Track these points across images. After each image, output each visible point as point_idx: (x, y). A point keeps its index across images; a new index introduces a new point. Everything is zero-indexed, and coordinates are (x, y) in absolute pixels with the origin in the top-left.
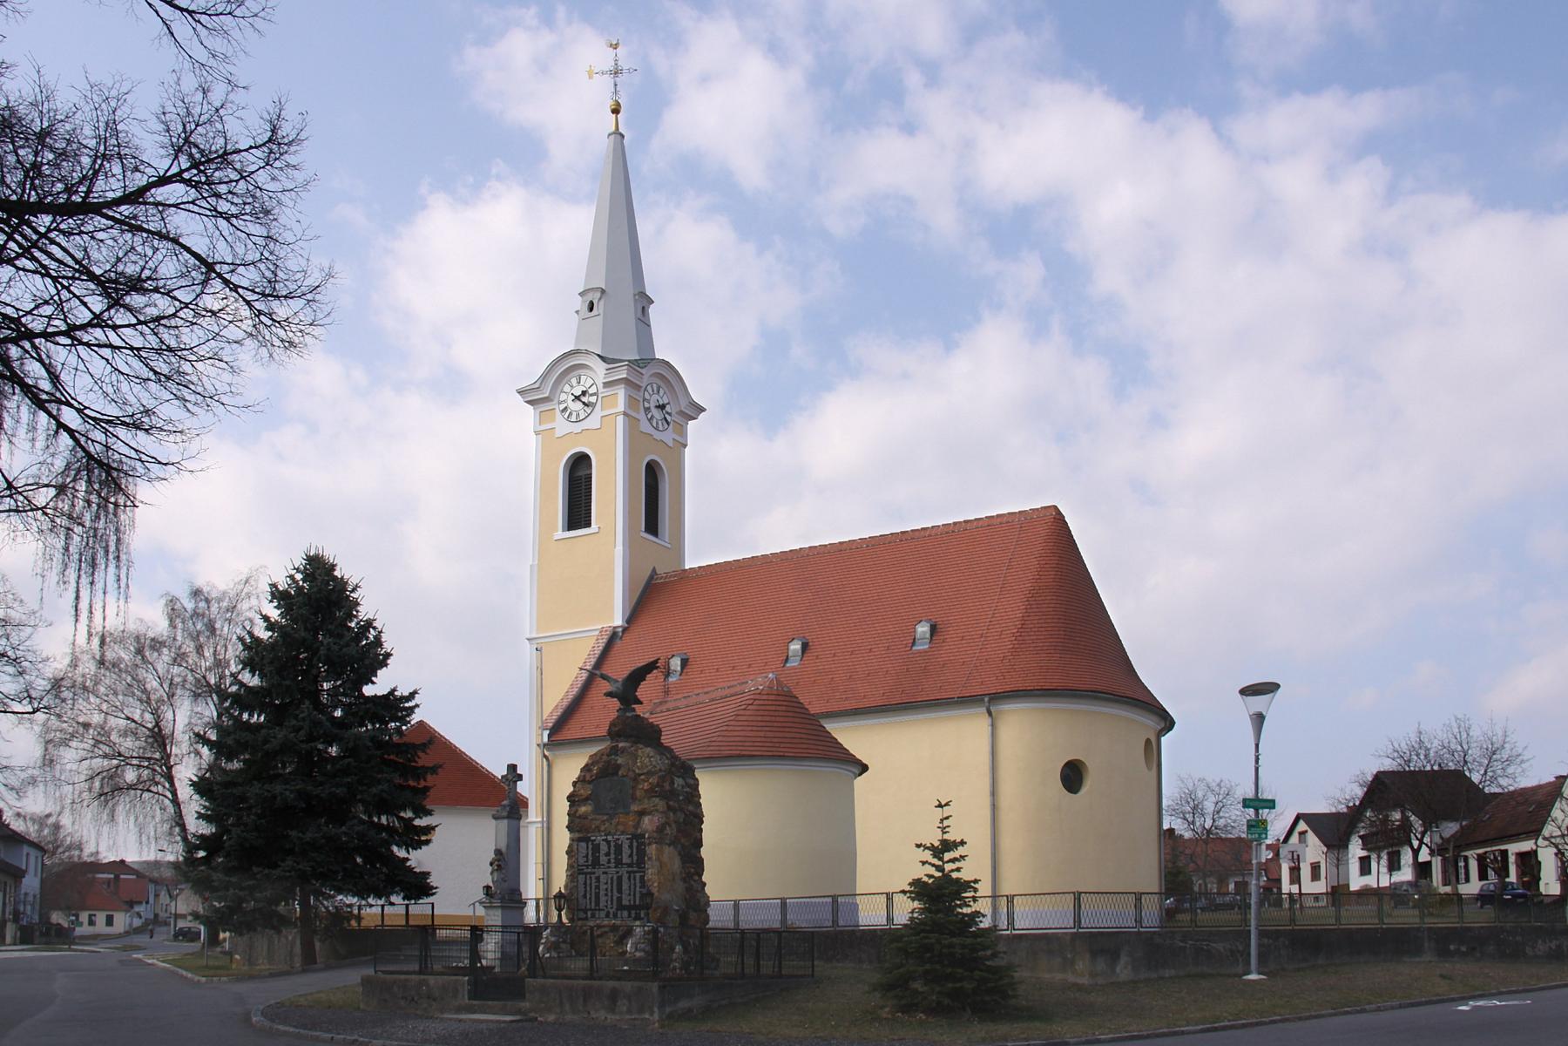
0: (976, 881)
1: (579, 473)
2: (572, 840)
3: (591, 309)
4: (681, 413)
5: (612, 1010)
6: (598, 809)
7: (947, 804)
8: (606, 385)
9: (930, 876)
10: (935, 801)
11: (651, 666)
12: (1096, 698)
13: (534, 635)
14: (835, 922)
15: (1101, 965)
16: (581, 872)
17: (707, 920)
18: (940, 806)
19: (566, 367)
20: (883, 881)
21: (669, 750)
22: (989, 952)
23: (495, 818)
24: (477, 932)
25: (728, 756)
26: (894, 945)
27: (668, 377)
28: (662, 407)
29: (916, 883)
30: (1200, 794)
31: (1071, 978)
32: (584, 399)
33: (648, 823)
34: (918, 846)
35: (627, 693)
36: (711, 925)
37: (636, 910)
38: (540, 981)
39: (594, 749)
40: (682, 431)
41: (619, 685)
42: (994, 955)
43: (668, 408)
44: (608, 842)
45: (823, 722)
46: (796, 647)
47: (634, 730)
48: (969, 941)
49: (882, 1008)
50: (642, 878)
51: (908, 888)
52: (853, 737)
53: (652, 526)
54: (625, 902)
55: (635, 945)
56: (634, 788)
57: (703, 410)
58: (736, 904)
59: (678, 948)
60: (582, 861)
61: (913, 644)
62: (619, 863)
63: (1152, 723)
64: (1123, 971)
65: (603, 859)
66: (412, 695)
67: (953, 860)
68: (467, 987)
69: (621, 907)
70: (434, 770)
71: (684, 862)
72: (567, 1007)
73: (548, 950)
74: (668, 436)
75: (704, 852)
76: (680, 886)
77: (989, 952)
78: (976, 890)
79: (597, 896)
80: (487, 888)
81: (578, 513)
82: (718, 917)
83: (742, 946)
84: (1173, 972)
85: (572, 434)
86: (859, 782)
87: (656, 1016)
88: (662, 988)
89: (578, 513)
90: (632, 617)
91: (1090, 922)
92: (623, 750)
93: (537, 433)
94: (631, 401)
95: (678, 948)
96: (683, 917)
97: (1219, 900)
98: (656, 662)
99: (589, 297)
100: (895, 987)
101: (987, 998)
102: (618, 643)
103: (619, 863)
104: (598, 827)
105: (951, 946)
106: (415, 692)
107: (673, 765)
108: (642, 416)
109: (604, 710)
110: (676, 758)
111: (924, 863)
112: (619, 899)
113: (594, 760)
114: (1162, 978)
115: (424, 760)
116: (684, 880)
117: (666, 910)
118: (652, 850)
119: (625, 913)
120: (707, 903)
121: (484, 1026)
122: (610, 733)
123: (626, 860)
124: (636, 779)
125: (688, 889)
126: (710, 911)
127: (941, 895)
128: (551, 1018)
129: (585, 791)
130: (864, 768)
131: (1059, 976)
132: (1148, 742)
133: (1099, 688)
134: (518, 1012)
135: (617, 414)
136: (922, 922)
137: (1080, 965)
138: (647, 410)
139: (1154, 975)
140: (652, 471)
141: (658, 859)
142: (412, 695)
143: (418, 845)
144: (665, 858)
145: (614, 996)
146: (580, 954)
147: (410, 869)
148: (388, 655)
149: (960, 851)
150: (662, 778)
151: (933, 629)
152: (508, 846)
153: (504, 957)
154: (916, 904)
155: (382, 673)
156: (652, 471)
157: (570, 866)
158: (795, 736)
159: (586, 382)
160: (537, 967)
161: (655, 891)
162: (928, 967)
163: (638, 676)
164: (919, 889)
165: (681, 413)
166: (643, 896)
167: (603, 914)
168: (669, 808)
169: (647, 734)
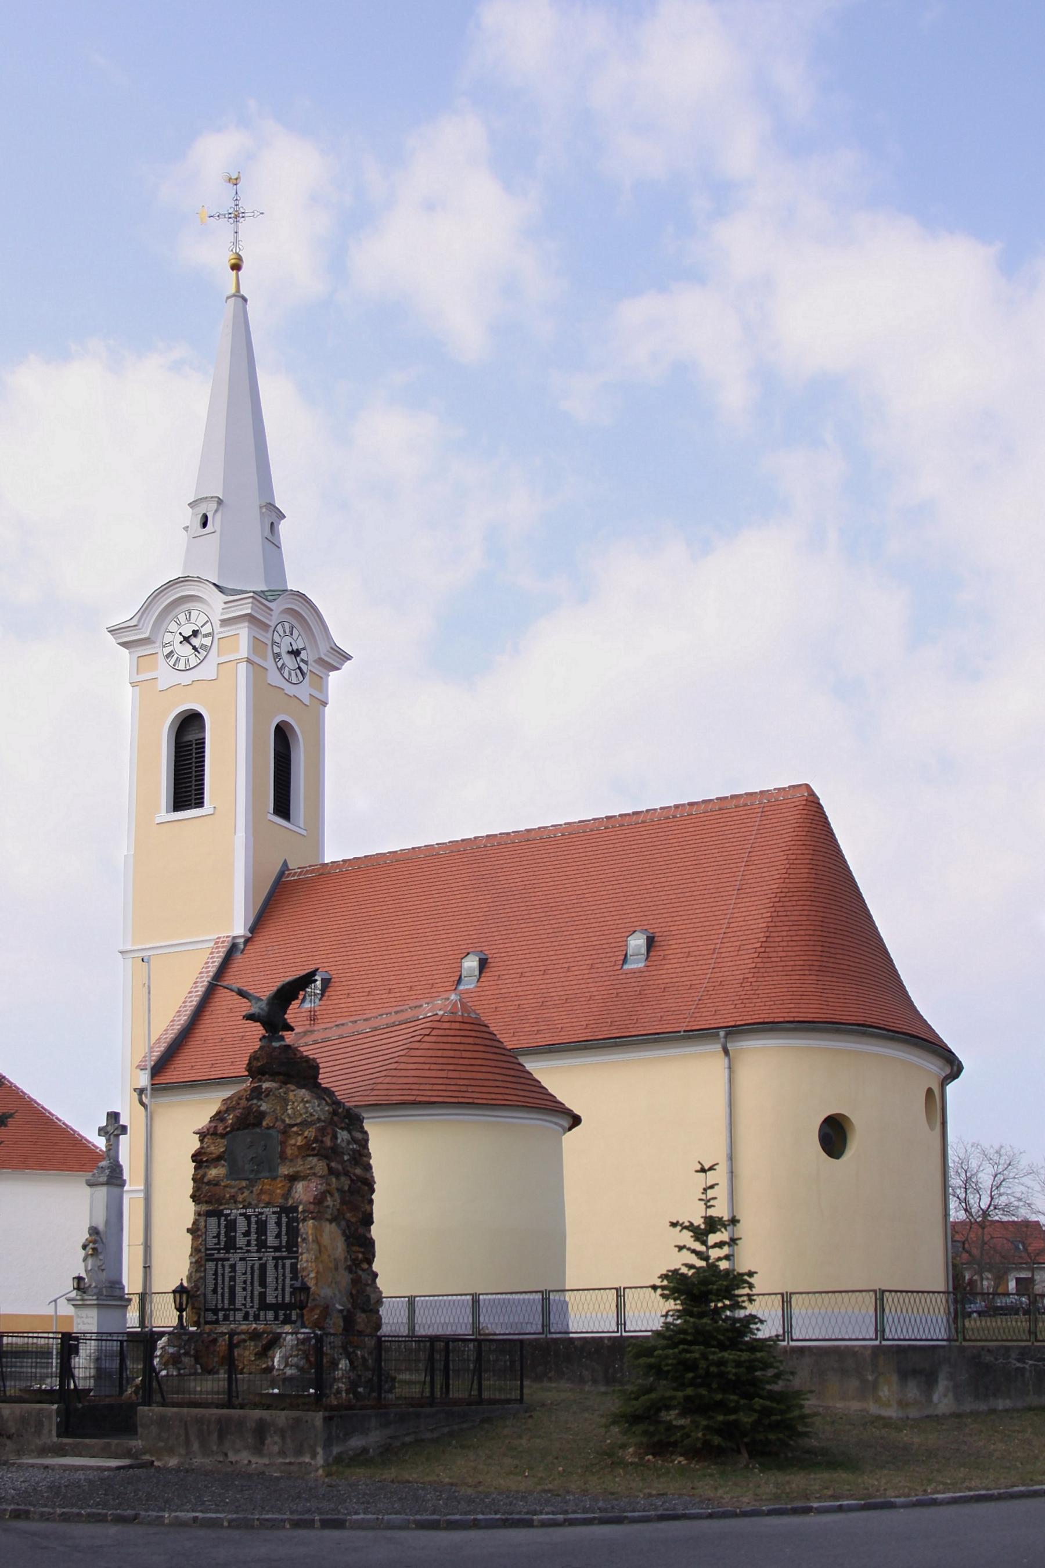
0: (751, 1274)
1: (188, 740)
2: (198, 1214)
3: (204, 525)
4: (321, 661)
5: (258, 1449)
6: (234, 1172)
7: (711, 1168)
8: (225, 622)
9: (690, 1267)
11: (308, 979)
12: (864, 1034)
13: (129, 948)
14: (621, 1322)
15: (913, 1391)
16: (209, 1258)
17: (379, 1326)
18: (703, 1170)
19: (171, 599)
20: (613, 1275)
22: (770, 1372)
23: (91, 1185)
24: (69, 1344)
25: (407, 1103)
26: (643, 1361)
27: (303, 613)
28: (296, 653)
29: (673, 1276)
30: (974, 1164)
31: (873, 1409)
32: (195, 642)
33: (303, 1192)
34: (674, 1225)
35: (273, 1016)
36: (385, 1330)
37: (284, 1311)
38: (157, 1409)
39: (227, 1093)
40: (320, 683)
41: (263, 1004)
42: (778, 1376)
43: (303, 655)
44: (248, 1218)
45: (522, 1060)
46: (471, 964)
47: (283, 1065)
48: (745, 1356)
49: (624, 1446)
50: (294, 1267)
51: (658, 1282)
52: (560, 1078)
53: (283, 807)
54: (270, 1299)
55: (285, 1359)
56: (283, 1143)
57: (348, 658)
58: (411, 1301)
59: (344, 1364)
60: (211, 1242)
61: (625, 960)
62: (262, 1245)
63: (935, 1068)
64: (943, 1400)
65: (241, 1241)
67: (720, 1245)
68: (55, 1420)
69: (264, 1306)
72: (196, 1446)
73: (165, 1365)
74: (303, 691)
75: (375, 1231)
76: (345, 1278)
77: (770, 1372)
78: (751, 1286)
79: (232, 1289)
80: (79, 1279)
81: (187, 789)
82: (392, 1319)
83: (431, 1360)
84: (1008, 1403)
85: (180, 689)
86: (571, 1139)
87: (320, 1460)
88: (328, 1420)
89: (187, 789)
90: (256, 927)
91: (898, 1332)
92: (269, 1092)
93: (134, 684)
94: (256, 644)
95: (344, 1364)
96: (349, 1320)
97: (999, 1302)
98: (313, 973)
99: (202, 509)
100: (641, 1418)
101: (772, 1437)
102: (239, 957)
103: (262, 1245)
104: (233, 1197)
105: (721, 1363)
107: (335, 1113)
108: (270, 664)
109: (236, 1039)
110: (338, 1103)
111: (681, 1248)
112: (263, 1296)
113: (229, 1106)
114: (993, 1411)
116: (349, 1269)
117: (326, 1310)
118: (307, 1228)
119: (270, 1315)
120: (379, 1301)
121: (80, 1475)
122: (250, 1068)
123: (271, 1241)
124: (285, 1132)
125: (356, 1282)
126: (382, 1311)
127: (706, 1292)
128: (173, 1462)
129: (217, 1148)
130: (576, 1121)
131: (855, 1406)
132: (930, 1092)
133: (869, 1021)
134: (128, 1454)
135: (238, 661)
136: (681, 1331)
137: (884, 1392)
138: (277, 656)
139: (1019, 1404)
140: (283, 736)
141: (316, 1241)
144: (326, 1240)
145: (261, 1431)
146: (209, 1371)
150: (322, 1131)
151: (651, 942)
152: (107, 1223)
153: (101, 1374)
154: (671, 1305)
156: (283, 736)
157: (195, 1250)
158: (487, 1076)
159: (198, 620)
160: (151, 1389)
161: (311, 1284)
162: (690, 1391)
163: (291, 991)
164: (676, 1284)
165: (321, 661)
166: (295, 1291)
167: (239, 1316)
168: (331, 1171)
169: (300, 1071)
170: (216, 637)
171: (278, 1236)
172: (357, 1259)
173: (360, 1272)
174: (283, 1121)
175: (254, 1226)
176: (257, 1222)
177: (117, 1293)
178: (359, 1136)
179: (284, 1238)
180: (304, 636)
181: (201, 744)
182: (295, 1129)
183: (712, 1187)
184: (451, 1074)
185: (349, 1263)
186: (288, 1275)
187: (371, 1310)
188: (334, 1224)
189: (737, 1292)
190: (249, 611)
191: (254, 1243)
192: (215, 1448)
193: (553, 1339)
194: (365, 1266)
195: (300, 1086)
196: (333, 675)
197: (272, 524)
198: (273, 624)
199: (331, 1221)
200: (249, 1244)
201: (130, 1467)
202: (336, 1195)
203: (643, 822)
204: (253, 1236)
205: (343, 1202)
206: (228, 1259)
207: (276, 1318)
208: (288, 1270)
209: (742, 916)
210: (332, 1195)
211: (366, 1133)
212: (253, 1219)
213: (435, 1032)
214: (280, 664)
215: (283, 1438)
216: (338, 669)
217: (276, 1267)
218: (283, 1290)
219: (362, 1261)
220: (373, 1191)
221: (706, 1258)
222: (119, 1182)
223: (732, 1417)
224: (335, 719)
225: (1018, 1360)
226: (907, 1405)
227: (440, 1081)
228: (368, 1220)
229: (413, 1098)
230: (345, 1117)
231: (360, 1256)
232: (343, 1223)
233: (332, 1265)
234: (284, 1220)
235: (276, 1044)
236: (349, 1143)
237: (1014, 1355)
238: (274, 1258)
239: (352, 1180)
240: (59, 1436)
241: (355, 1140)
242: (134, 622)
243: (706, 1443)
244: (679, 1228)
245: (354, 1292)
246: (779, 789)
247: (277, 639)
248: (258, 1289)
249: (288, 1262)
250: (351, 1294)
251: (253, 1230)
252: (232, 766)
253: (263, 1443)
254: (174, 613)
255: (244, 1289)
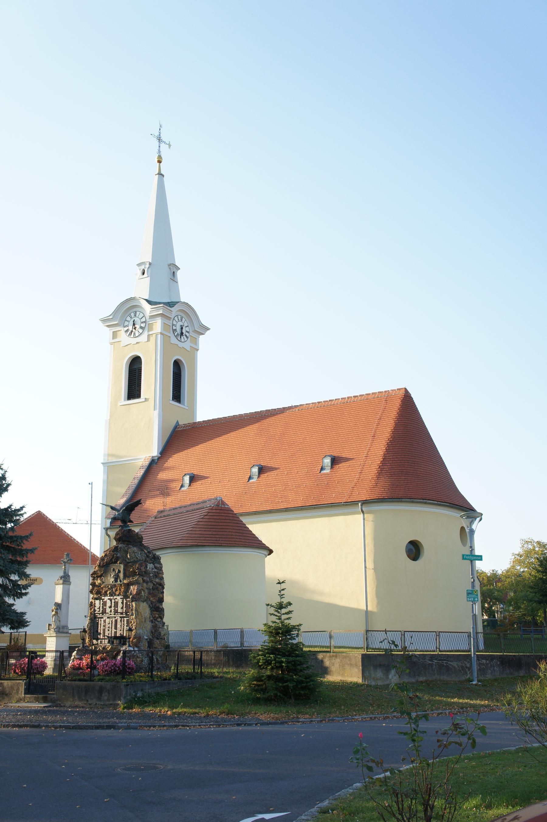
1: (135, 368)
3: (143, 274)
7: (283, 582)
8: (152, 317)
10: (325, 567)
18: (279, 583)
21: (146, 548)
27: (188, 312)
34: (268, 605)
44: (111, 600)
53: (177, 396)
57: (208, 329)
62: (116, 612)
65: (108, 610)
66: (22, 508)
67: (286, 613)
70: (32, 551)
71: (152, 611)
72: (76, 698)
74: (187, 345)
76: (149, 625)
81: (134, 390)
89: (134, 390)
93: (111, 344)
94: (164, 326)
96: (150, 643)
99: (142, 267)
101: (302, 692)
102: (155, 466)
103: (116, 612)
106: (23, 507)
115: (26, 545)
116: (152, 621)
123: (120, 610)
130: (271, 552)
132: (462, 529)
140: (177, 366)
142: (22, 508)
143: (21, 595)
144: (141, 609)
147: (15, 612)
148: (9, 485)
149: (290, 608)
155: (5, 495)
156: (177, 366)
170: (147, 323)
171: (122, 608)
172: (155, 617)
173: (157, 623)
174: (126, 561)
175: (113, 604)
176: (114, 602)
177: (65, 631)
178: (158, 565)
179: (124, 609)
180: (187, 320)
181: (140, 370)
182: (130, 564)
183: (283, 590)
184: (214, 533)
185: (151, 619)
186: (126, 625)
187: (161, 638)
188: (145, 603)
189: (292, 633)
190: (161, 312)
191: (113, 611)
192: (83, 698)
193: (244, 650)
194: (159, 620)
195: (134, 546)
196: (201, 337)
197: (174, 272)
198: (173, 317)
199: (143, 602)
200: (111, 611)
201: (50, 706)
202: (146, 591)
203: (333, 405)
204: (113, 608)
205: (149, 593)
206: (102, 618)
207: (120, 643)
208: (125, 622)
209: (370, 451)
210: (144, 591)
211: (161, 564)
212: (113, 601)
213: (209, 514)
214: (176, 334)
215: (109, 693)
216: (203, 334)
217: (121, 621)
218: (123, 631)
219: (157, 618)
220: (163, 588)
221: (280, 619)
222: (68, 583)
223: (285, 684)
224: (201, 356)
225: (430, 660)
226: (377, 679)
227: (209, 536)
228: (161, 600)
229: (196, 544)
230: (152, 558)
231: (157, 616)
232: (149, 602)
233: (143, 620)
234: (125, 601)
235: (125, 529)
236: (152, 569)
237: (427, 658)
238: (120, 617)
239: (154, 584)
240: (25, 694)
241: (156, 568)
242: (111, 317)
243: (276, 695)
244: (269, 606)
245: (153, 631)
246: (393, 390)
247: (175, 323)
248: (114, 630)
249: (125, 619)
250: (152, 632)
251: (113, 606)
252: (152, 380)
253: (101, 696)
254: (129, 313)
255: (109, 630)
